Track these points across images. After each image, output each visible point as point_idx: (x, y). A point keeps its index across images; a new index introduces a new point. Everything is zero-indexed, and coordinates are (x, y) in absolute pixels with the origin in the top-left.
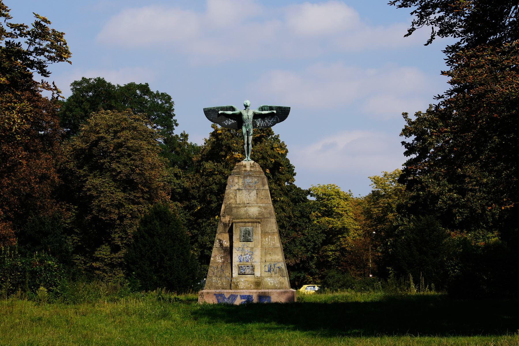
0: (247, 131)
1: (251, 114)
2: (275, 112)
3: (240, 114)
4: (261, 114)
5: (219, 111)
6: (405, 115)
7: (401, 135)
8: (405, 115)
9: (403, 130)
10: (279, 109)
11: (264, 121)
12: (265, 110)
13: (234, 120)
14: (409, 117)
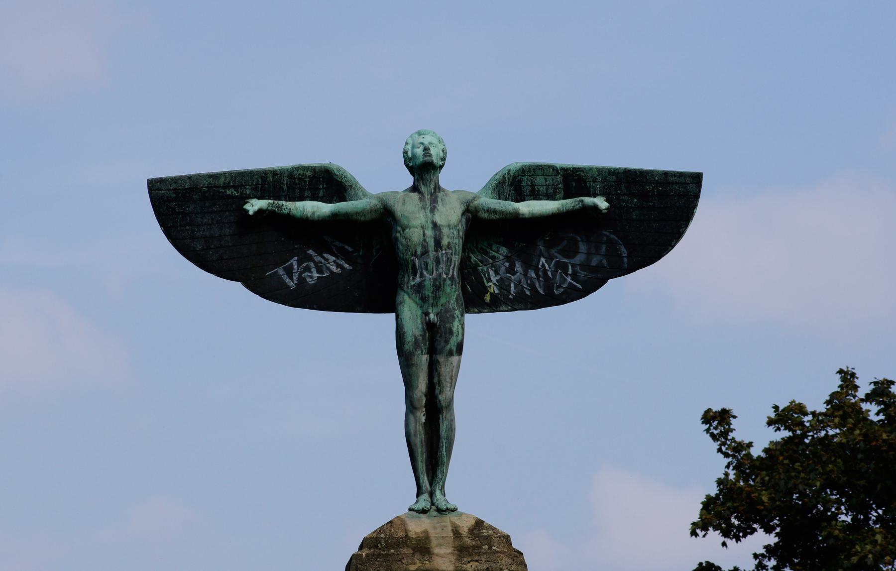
0: (430, 327)
1: (450, 215)
2: (602, 203)
3: (385, 219)
4: (516, 219)
5: (244, 199)
6: (718, 421)
7: (700, 527)
8: (718, 421)
9: (709, 504)
10: (627, 184)
11: (528, 264)
12: (535, 195)
13: (340, 253)
14: (740, 432)
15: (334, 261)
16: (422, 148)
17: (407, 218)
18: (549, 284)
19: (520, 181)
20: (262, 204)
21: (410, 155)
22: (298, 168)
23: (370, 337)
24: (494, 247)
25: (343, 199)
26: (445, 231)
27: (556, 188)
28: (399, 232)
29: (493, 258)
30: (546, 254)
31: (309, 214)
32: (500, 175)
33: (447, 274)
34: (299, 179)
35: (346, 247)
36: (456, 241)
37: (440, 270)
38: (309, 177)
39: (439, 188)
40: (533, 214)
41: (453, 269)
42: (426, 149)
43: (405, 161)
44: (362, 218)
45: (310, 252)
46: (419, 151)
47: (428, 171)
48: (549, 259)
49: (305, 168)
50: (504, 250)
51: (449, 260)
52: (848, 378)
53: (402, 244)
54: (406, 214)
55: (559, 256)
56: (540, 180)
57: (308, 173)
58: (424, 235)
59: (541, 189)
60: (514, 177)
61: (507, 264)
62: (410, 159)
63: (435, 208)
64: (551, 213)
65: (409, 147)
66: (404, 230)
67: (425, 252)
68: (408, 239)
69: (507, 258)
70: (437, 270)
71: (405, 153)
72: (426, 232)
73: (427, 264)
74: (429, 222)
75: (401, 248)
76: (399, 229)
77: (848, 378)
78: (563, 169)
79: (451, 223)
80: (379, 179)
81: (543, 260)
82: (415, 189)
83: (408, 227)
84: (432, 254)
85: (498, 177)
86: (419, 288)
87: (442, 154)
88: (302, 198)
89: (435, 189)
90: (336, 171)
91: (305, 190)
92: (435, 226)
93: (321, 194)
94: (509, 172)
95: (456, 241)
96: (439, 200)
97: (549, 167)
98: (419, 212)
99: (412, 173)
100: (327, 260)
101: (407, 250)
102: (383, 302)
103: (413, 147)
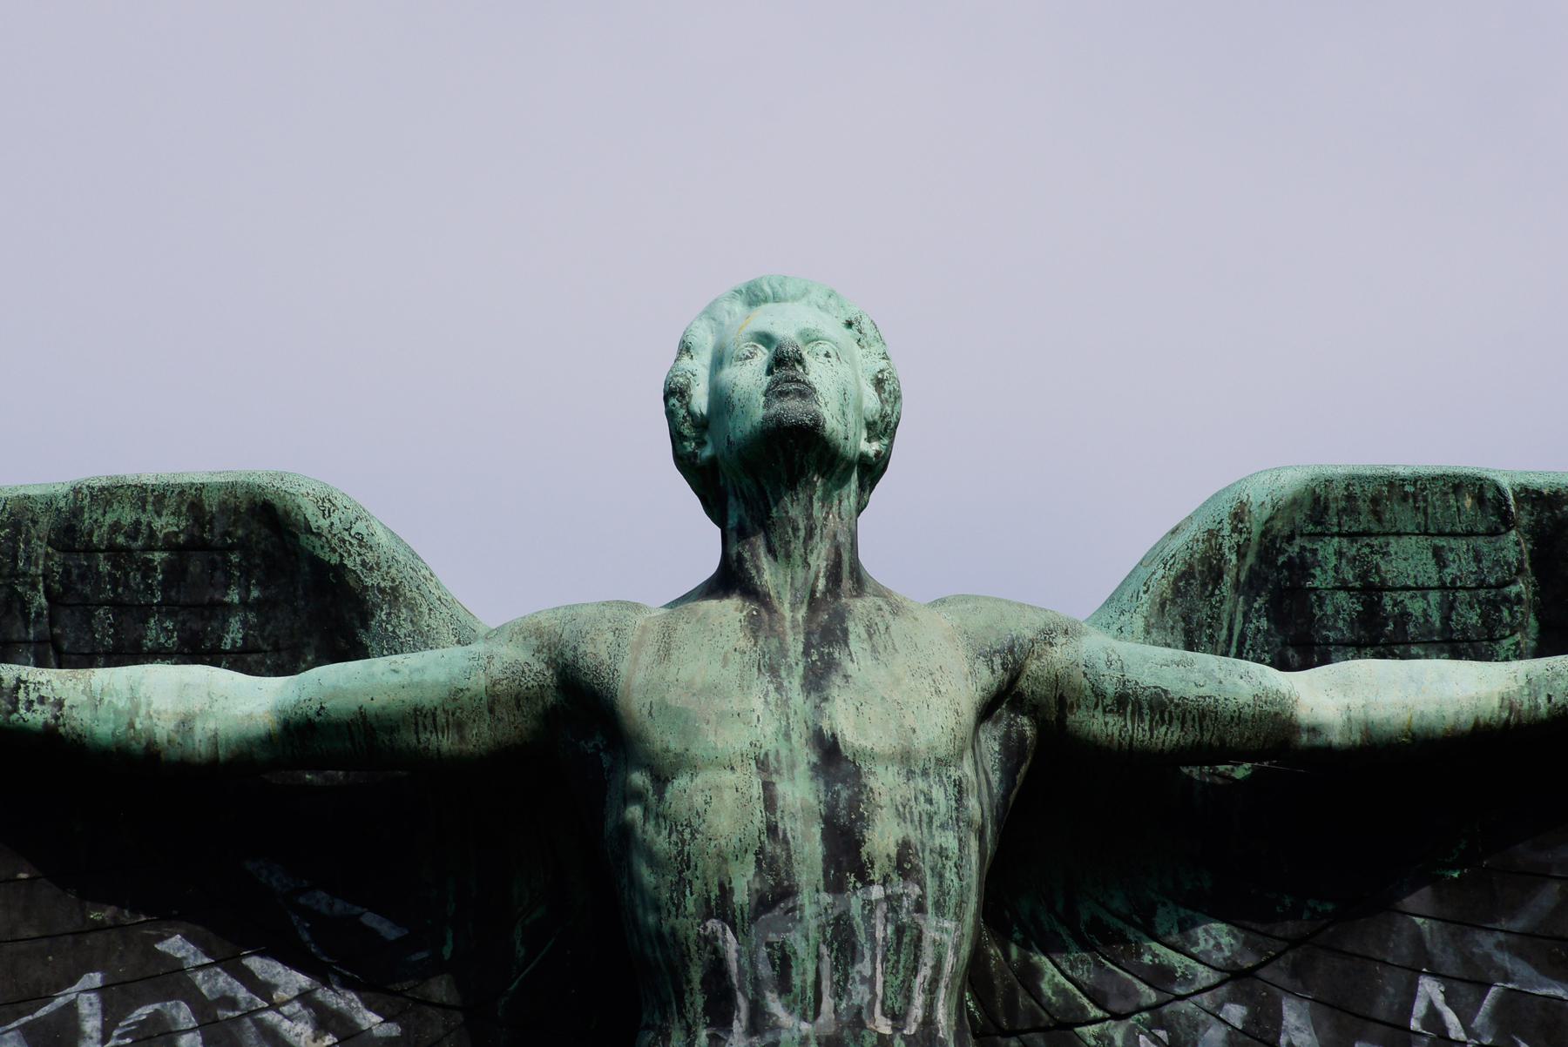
1: (912, 702)
3: (575, 735)
12: (1381, 635)
15: (304, 997)
16: (763, 356)
17: (682, 720)
19: (1302, 567)
21: (700, 401)
22: (107, 495)
24: (1164, 919)
25: (357, 651)
26: (885, 783)
27: (1494, 602)
28: (638, 796)
29: (1161, 977)
30: (1449, 961)
31: (163, 729)
32: (1194, 530)
33: (898, 1018)
34: (113, 550)
35: (370, 919)
36: (949, 841)
37: (860, 994)
38: (170, 544)
39: (860, 582)
40: (1368, 729)
41: (934, 983)
42: (784, 362)
43: (677, 437)
44: (446, 743)
45: (175, 945)
46: (749, 377)
47: (794, 479)
48: (1466, 985)
49: (149, 497)
50: (1217, 939)
51: (907, 941)
53: (652, 859)
54: (674, 698)
55: (1523, 970)
56: (1407, 560)
57: (165, 524)
58: (770, 802)
59: (1416, 606)
60: (1270, 544)
61: (1236, 1013)
62: (702, 425)
63: (830, 665)
64: (1466, 720)
65: (698, 370)
66: (661, 780)
67: (777, 895)
68: (686, 827)
69: (1236, 978)
70: (841, 991)
71: (675, 393)
72: (782, 788)
73: (783, 962)
74: (799, 738)
75: (647, 876)
76: (639, 779)
78: (1529, 496)
79: (920, 743)
80: (528, 539)
81: (1430, 990)
82: (730, 579)
83: (683, 763)
84: (812, 901)
85: (1179, 542)
87: (871, 403)
88: (128, 652)
89: (834, 576)
90: (311, 511)
91: (145, 612)
92: (830, 755)
93: (234, 634)
94: (1238, 516)
95: (949, 841)
96: (856, 629)
97: (1457, 485)
98: (744, 688)
99: (715, 506)
100: (263, 989)
101: (681, 884)
103: (718, 362)
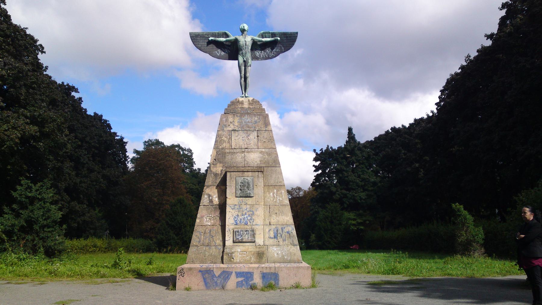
0: (244, 61)
2: (279, 39)
6: (315, 150)
10: (285, 35)
18: (268, 55)
20: (213, 38)
23: (233, 65)
52: (328, 146)
56: (267, 35)
77: (328, 146)
86: (242, 53)
102: (236, 58)
